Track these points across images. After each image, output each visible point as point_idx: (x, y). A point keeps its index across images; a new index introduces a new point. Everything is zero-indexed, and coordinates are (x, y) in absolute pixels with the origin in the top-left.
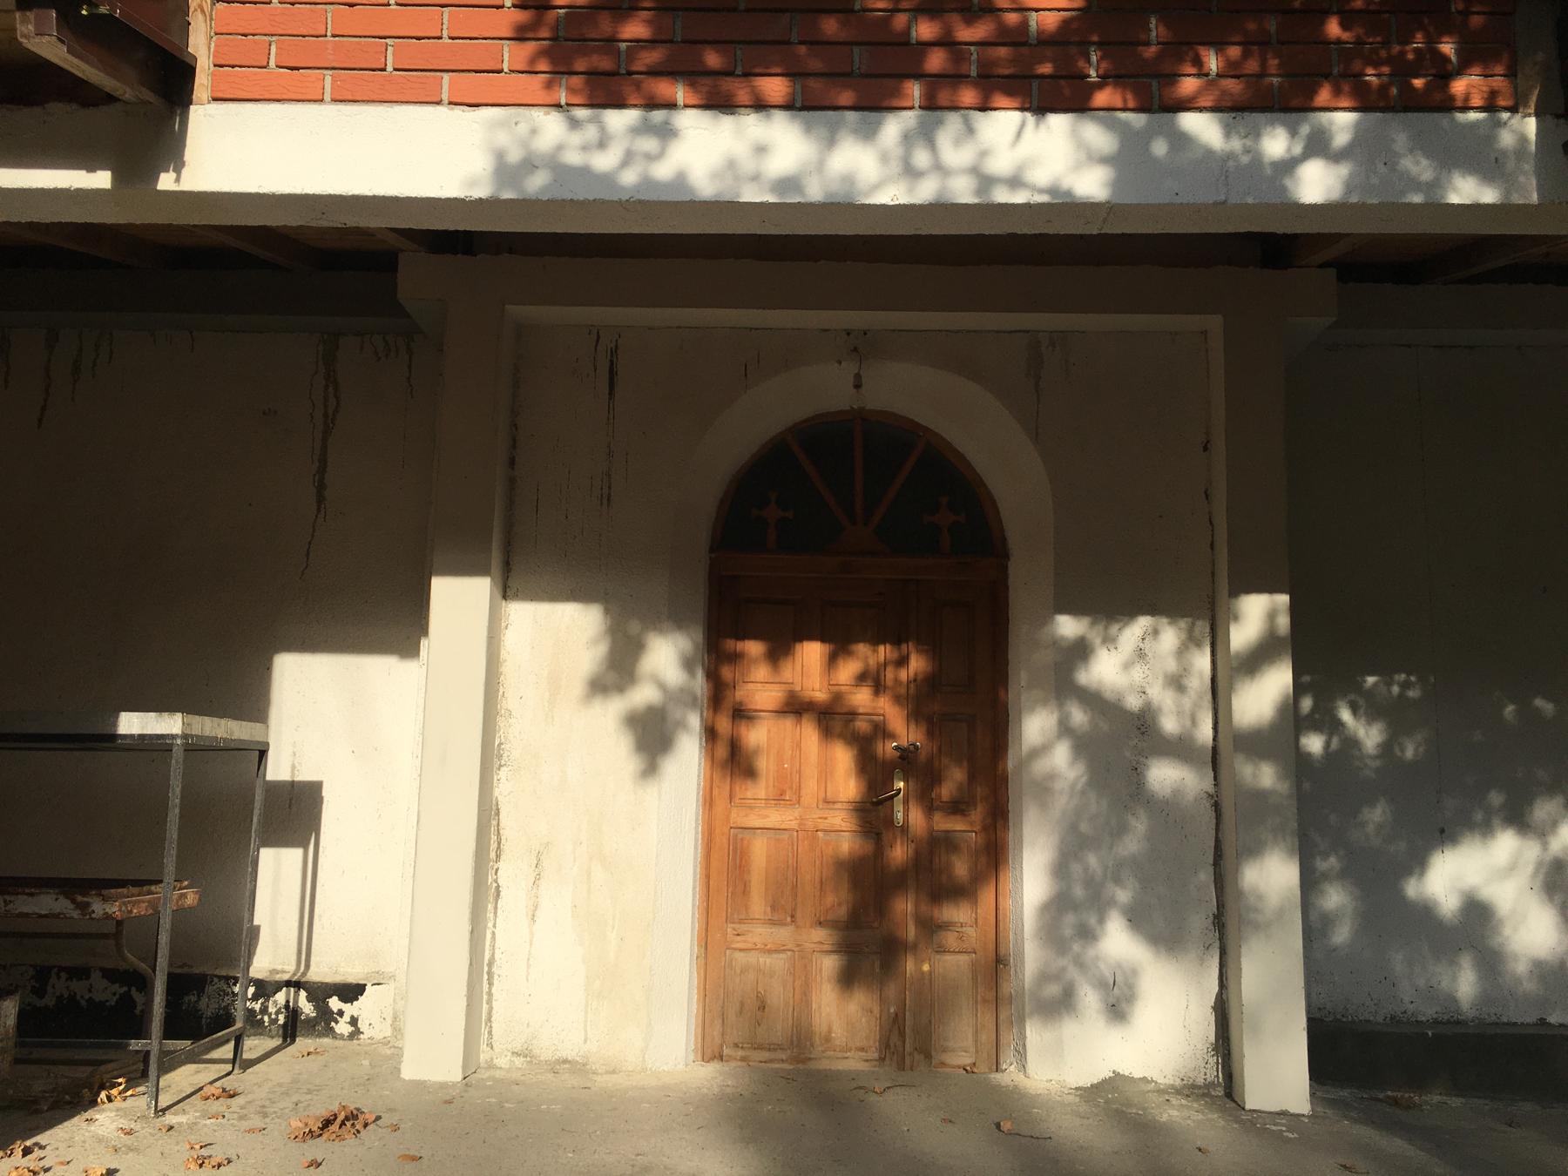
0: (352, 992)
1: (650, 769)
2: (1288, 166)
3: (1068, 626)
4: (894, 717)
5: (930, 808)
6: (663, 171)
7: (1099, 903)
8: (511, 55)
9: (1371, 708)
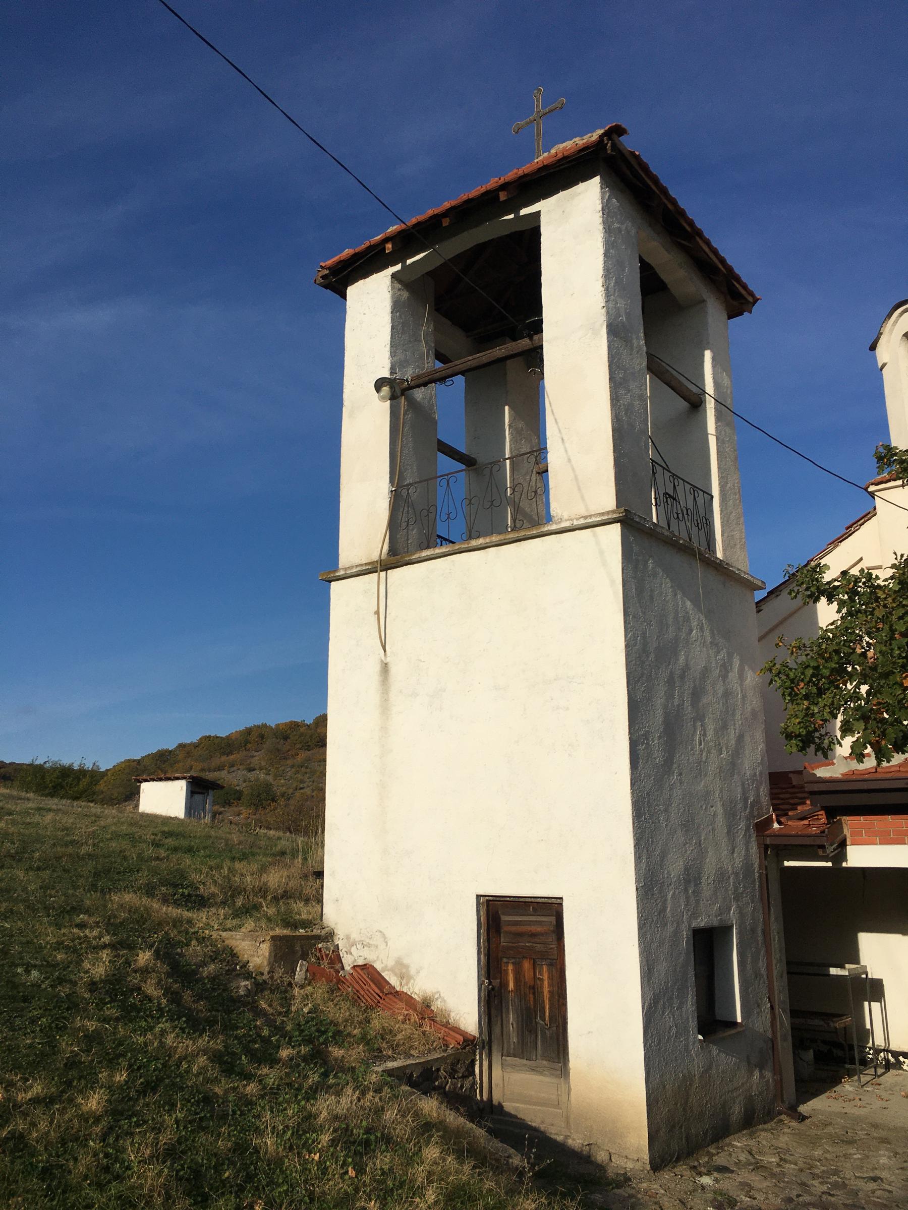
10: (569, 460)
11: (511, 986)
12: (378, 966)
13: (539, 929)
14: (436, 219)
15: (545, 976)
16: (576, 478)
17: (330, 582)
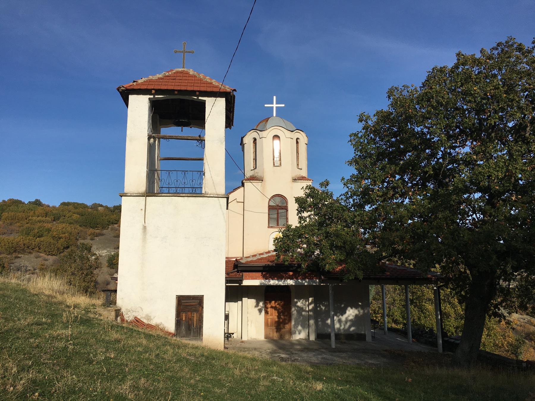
0: (233, 334)
1: (260, 314)
2: (304, 283)
3: (296, 300)
4: (280, 307)
5: (284, 316)
6: (270, 284)
7: (298, 324)
8: (261, 277)
9: (323, 305)
10: (212, 177)
11: (184, 319)
12: (139, 317)
13: (194, 304)
14: (174, 90)
15: (195, 316)
16: (213, 182)
17: (121, 196)
